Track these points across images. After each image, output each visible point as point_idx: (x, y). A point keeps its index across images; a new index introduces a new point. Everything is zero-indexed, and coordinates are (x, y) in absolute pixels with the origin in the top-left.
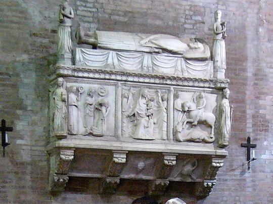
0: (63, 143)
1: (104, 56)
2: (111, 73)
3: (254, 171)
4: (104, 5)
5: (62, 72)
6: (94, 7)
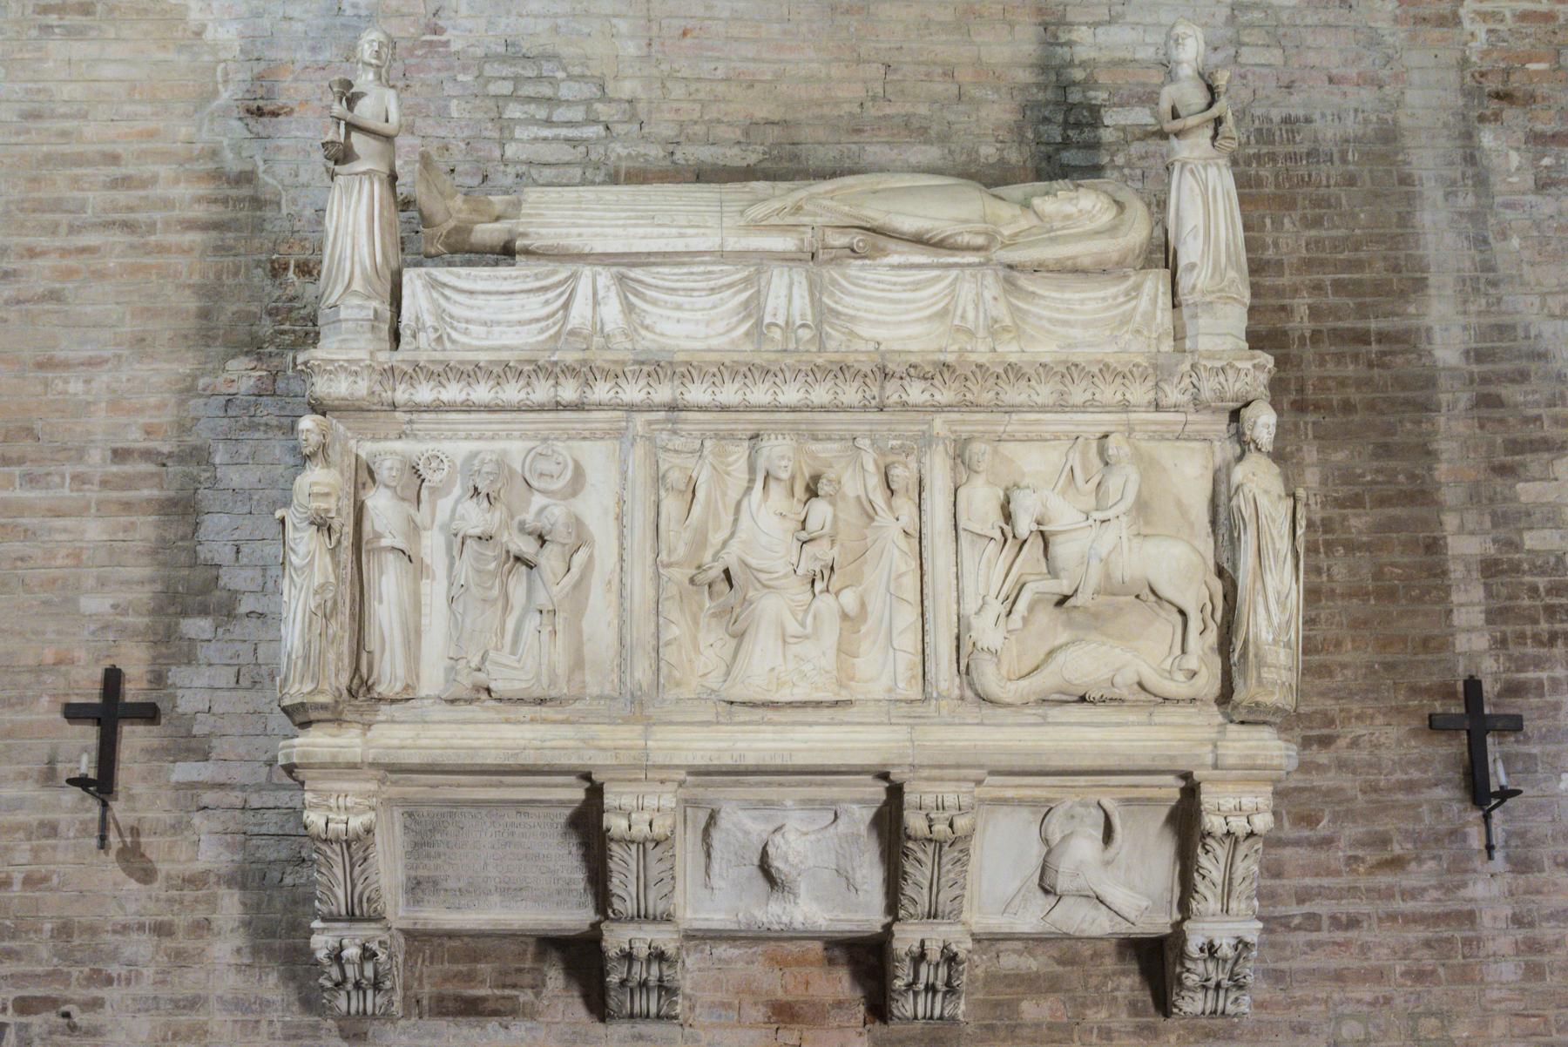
0: (317, 742)
1: (551, 295)
2: (585, 373)
3: (1522, 865)
4: (642, 107)
5: (322, 387)
6: (592, 121)
